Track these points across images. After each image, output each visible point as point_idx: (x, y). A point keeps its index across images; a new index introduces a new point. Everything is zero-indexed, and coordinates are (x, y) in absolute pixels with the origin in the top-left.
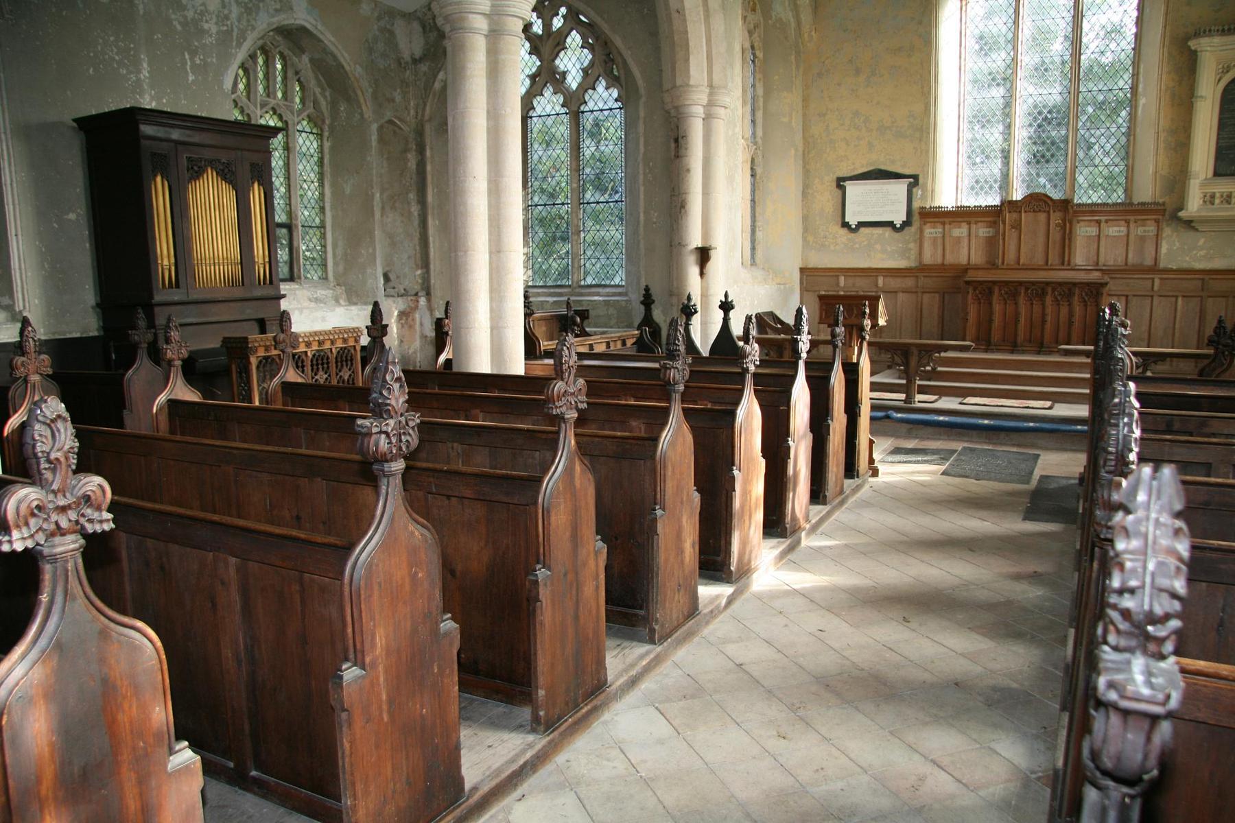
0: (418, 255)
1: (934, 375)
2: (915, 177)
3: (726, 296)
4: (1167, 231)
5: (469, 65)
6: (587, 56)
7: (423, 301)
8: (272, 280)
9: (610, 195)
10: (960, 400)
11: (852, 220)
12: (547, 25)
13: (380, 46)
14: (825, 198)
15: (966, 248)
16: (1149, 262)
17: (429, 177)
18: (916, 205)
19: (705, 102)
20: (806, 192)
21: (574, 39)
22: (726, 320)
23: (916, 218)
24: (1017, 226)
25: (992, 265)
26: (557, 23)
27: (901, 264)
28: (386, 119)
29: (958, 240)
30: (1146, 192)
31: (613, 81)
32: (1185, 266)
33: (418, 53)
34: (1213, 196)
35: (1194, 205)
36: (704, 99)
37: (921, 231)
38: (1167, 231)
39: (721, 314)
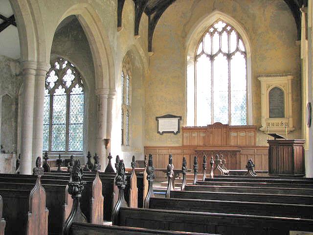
0: (14, 140)
2: (180, 117)
4: (258, 134)
5: (30, 84)
6: (73, 77)
7: (14, 155)
8: (182, 130)
9: (225, 108)
11: (161, 131)
12: (61, 66)
13: (5, 70)
14: (152, 123)
15: (197, 141)
16: (253, 144)
17: (19, 114)
18: (181, 126)
19: (108, 93)
20: (146, 122)
21: (69, 71)
23: (181, 130)
25: (205, 145)
26: (64, 66)
28: (5, 94)
29: (250, 137)
30: (251, 123)
31: (81, 85)
32: (264, 145)
33: (18, 73)
35: (264, 125)
37: (183, 135)
38: (258, 134)
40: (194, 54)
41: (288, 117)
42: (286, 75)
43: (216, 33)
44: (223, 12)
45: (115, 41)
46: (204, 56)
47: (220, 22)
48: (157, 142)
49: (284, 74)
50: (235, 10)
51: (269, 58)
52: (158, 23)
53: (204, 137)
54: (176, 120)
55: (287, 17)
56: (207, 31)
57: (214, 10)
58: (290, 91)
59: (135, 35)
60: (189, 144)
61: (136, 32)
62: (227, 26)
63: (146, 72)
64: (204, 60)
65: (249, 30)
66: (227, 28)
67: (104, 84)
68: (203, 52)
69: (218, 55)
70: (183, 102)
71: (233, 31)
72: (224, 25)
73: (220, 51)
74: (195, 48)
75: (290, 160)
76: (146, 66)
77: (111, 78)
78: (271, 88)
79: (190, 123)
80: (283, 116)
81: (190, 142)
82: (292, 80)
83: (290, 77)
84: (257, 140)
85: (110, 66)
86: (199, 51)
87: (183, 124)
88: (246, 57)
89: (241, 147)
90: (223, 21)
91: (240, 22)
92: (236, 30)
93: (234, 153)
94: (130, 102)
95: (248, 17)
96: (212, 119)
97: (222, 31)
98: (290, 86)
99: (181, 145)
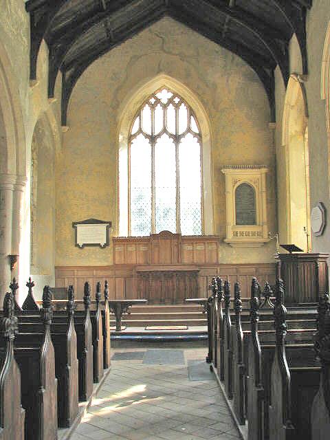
1: (129, 316)
2: (110, 223)
3: (30, 279)
8: (114, 242)
10: (144, 328)
11: (80, 243)
14: (67, 232)
15: (136, 257)
18: (111, 235)
19: (14, 183)
20: (57, 229)
22: (30, 292)
23: (111, 242)
24: (157, 246)
27: (105, 264)
30: (210, 231)
32: (228, 263)
34: (237, 233)
35: (230, 237)
36: (14, 181)
37: (114, 249)
39: (28, 289)
40: (127, 133)
41: (261, 224)
42: (260, 168)
43: (159, 105)
44: (172, 76)
45: (27, 100)
46: (141, 137)
47: (164, 91)
48: (76, 259)
49: (256, 165)
50: (188, 75)
51: (234, 143)
52: (76, 85)
53: (145, 252)
54: (103, 228)
55: (256, 90)
56: (147, 102)
57: (159, 72)
58: (264, 189)
59: (49, 97)
60: (123, 263)
61: (51, 94)
62: (174, 97)
63: (57, 155)
64: (141, 143)
65: (208, 101)
66: (174, 100)
67: (9, 167)
68: (140, 131)
69: (138, 137)
70: (113, 200)
71: (183, 104)
72: (170, 95)
73: (165, 131)
74: (129, 125)
75: (313, 279)
76: (58, 146)
77: (20, 159)
78: (238, 184)
79: (123, 233)
80: (254, 223)
81: (124, 261)
82: (266, 173)
83: (264, 170)
84: (220, 256)
85: (18, 140)
86: (135, 130)
87: (114, 232)
88: (200, 141)
89: (199, 266)
90: (169, 90)
91: (196, 91)
92: (186, 103)
93: (194, 274)
94: (35, 200)
95: (207, 86)
96: (153, 227)
97: (168, 104)
98: (264, 183)
99: (112, 264)
